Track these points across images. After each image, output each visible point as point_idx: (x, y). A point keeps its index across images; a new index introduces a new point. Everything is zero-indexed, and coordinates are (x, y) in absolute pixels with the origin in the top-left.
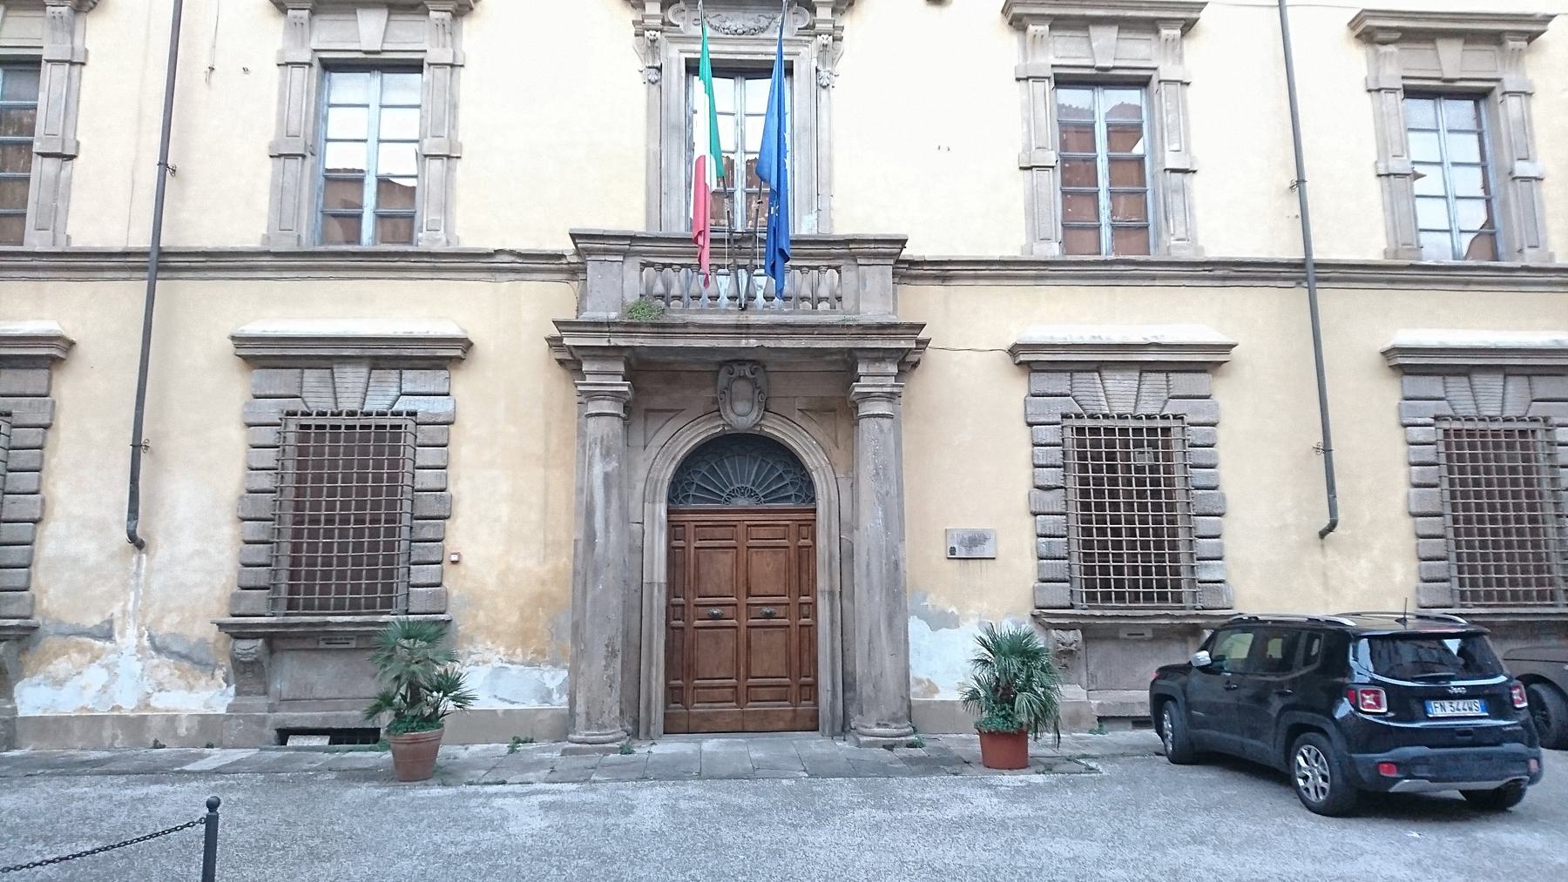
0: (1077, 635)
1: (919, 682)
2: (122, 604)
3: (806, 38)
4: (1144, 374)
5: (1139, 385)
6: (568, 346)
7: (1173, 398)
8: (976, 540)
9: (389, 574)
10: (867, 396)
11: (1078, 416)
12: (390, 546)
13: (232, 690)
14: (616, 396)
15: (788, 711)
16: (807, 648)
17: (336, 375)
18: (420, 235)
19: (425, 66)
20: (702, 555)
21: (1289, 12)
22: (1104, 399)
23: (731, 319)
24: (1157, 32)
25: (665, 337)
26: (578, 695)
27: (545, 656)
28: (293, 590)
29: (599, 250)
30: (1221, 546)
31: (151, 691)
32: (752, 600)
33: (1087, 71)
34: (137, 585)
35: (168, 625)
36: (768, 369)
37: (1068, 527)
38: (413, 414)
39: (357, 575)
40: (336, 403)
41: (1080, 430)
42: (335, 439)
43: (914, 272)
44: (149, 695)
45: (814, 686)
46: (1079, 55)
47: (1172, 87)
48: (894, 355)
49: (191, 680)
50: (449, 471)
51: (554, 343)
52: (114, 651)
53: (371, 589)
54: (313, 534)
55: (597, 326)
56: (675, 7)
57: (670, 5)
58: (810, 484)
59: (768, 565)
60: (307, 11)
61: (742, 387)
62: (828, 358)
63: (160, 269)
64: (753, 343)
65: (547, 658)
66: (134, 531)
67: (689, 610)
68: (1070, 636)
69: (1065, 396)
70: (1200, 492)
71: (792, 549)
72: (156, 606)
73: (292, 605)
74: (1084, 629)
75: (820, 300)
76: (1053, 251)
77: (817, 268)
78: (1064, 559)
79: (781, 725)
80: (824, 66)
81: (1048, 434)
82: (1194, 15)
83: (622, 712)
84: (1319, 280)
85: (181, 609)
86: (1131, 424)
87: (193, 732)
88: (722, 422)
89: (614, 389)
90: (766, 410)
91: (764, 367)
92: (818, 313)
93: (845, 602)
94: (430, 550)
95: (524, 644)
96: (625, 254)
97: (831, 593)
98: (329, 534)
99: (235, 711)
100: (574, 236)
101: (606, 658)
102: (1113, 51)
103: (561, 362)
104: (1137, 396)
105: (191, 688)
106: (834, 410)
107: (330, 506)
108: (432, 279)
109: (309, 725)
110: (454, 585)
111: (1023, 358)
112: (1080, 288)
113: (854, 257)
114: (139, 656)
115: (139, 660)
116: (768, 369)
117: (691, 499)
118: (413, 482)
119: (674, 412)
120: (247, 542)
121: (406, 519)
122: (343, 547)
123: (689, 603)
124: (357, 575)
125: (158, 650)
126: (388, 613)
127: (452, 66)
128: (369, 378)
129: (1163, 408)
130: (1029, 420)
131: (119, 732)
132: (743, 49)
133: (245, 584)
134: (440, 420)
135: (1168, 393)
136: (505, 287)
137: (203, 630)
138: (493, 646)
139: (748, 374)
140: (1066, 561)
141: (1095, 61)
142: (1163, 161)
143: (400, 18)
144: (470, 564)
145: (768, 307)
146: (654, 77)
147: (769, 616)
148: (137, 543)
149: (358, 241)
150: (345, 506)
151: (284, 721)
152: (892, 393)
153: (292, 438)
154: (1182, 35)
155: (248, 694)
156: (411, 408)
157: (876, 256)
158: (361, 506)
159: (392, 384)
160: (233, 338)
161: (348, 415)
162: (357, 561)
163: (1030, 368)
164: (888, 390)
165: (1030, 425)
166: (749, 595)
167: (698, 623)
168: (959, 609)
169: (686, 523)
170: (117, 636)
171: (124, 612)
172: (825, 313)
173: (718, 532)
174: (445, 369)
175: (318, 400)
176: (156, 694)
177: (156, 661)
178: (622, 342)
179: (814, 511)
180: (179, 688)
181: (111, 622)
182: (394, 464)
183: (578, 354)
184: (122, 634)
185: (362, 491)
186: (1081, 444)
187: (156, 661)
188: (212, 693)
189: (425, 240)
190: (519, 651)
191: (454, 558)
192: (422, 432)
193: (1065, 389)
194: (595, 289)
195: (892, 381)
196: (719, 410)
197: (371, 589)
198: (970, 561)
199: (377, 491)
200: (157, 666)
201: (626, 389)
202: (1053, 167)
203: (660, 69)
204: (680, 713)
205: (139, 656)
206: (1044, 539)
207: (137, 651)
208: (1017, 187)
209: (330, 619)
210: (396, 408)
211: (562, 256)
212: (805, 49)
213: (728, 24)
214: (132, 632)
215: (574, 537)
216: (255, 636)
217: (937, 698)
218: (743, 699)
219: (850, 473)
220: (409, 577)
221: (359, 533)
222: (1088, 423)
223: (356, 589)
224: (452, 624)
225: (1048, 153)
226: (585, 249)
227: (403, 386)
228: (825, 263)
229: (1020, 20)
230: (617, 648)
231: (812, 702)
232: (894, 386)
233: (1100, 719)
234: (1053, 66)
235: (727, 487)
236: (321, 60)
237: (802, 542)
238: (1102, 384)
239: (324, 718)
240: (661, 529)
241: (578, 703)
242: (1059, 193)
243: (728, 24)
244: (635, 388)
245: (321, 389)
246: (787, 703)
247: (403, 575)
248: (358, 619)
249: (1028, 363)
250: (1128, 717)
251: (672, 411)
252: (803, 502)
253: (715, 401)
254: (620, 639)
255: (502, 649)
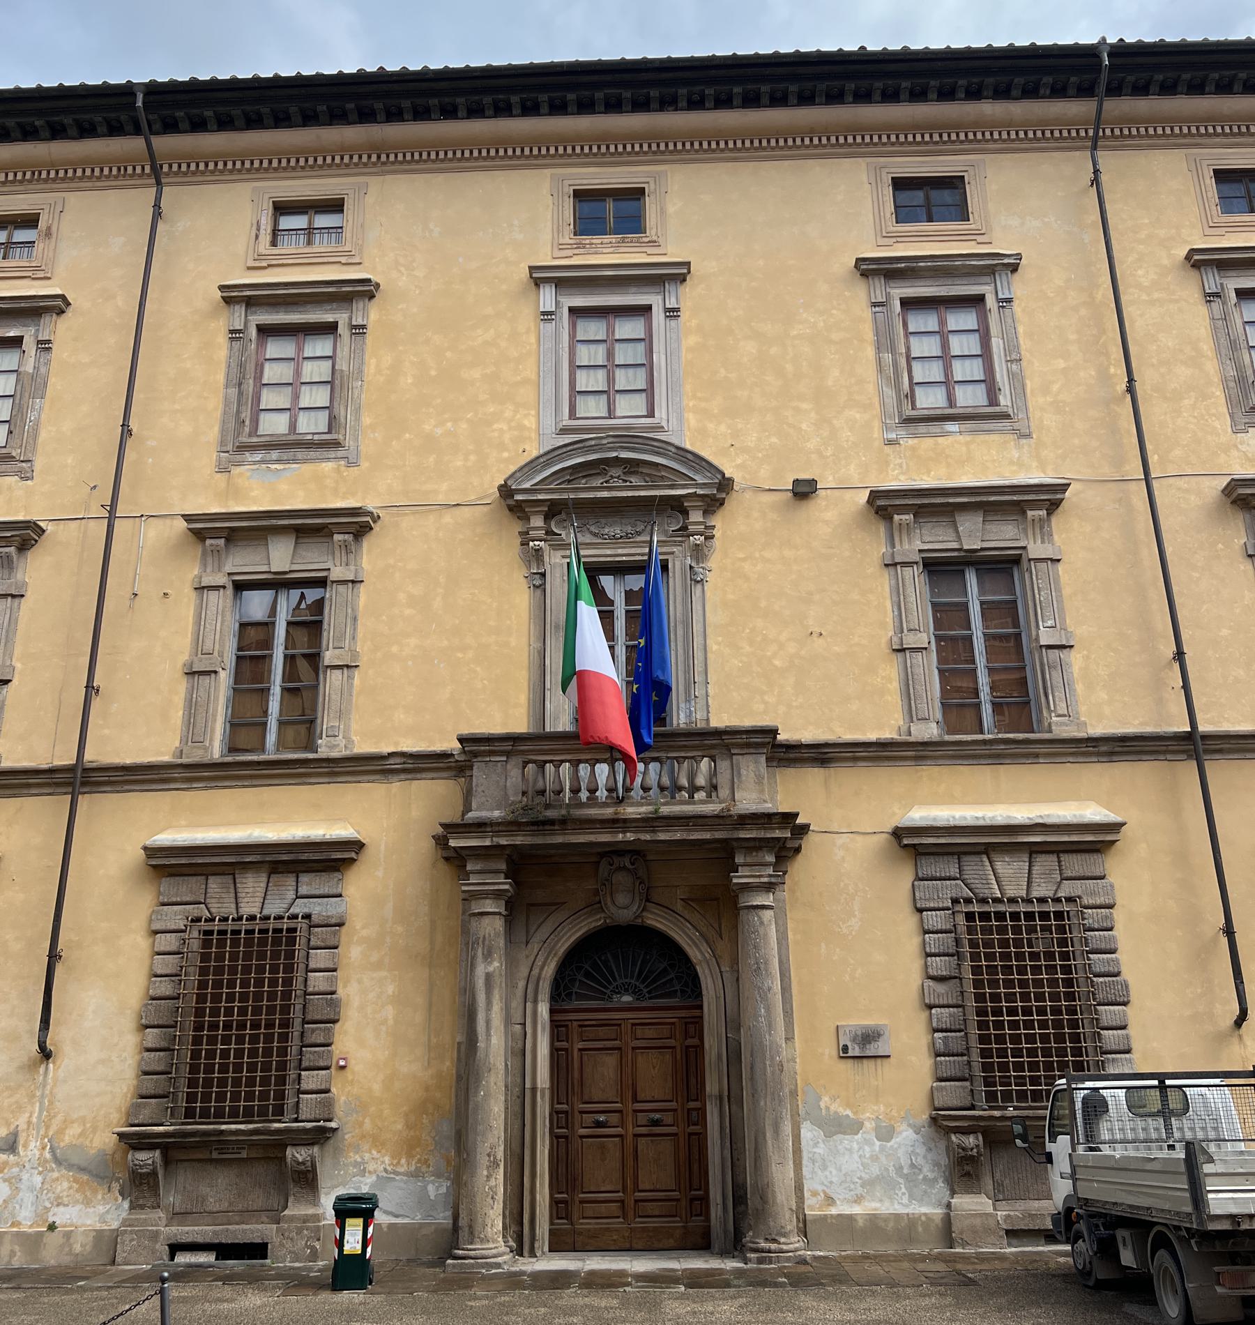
0: (978, 1139)
1: (815, 1194)
2: (27, 1115)
3: (680, 539)
4: (1034, 856)
5: (1030, 866)
6: (454, 848)
7: (1067, 879)
8: (869, 1037)
9: (282, 1081)
10: (747, 888)
11: (968, 901)
12: (283, 1052)
13: (126, 1205)
14: (497, 895)
15: (677, 1227)
16: (697, 1157)
17: (237, 881)
18: (320, 741)
19: (329, 583)
20: (585, 1058)
21: (1155, 484)
22: (994, 882)
23: (608, 812)
24: (1024, 513)
25: (544, 835)
26: (461, 1206)
27: (429, 1166)
28: (191, 1098)
29: (484, 751)
30: (1127, 1037)
31: (48, 1205)
32: (638, 1106)
33: (955, 554)
34: (43, 1096)
35: (71, 1135)
36: (648, 858)
37: (965, 1020)
38: (307, 917)
39: (251, 1082)
40: (237, 909)
41: (970, 916)
42: (235, 943)
43: (792, 756)
44: (47, 1210)
45: (705, 1200)
46: (945, 539)
47: (1042, 566)
48: (771, 845)
49: (88, 1193)
50: (338, 974)
51: (441, 841)
52: (17, 1164)
53: (264, 1096)
54: (212, 1040)
55: (480, 827)
56: (558, 517)
57: (553, 516)
58: (696, 977)
59: (654, 1068)
60: (223, 540)
61: (621, 878)
62: (707, 846)
63: (83, 784)
64: (630, 836)
65: (431, 1169)
66: (45, 1042)
67: (573, 1117)
68: (971, 1141)
69: (954, 879)
70: (1101, 979)
71: (678, 1051)
72: (60, 1117)
73: (189, 1113)
74: (986, 1133)
75: (698, 789)
76: (929, 731)
77: (692, 758)
78: (962, 1055)
79: (671, 1242)
80: (698, 563)
81: (936, 920)
82: (1059, 496)
83: (504, 1227)
84: (1206, 751)
85: (83, 1120)
86: (1023, 908)
87: (88, 1248)
88: (603, 915)
89: (496, 887)
90: (648, 900)
91: (645, 856)
92: (694, 803)
93: (734, 1107)
94: (320, 1055)
95: (410, 1156)
96: (508, 754)
97: (721, 1098)
98: (226, 1040)
99: (130, 1226)
100: (462, 740)
101: (488, 1167)
102: (979, 534)
103: (447, 859)
104: (1029, 878)
105: (87, 1203)
106: (717, 899)
107: (229, 1012)
108: (329, 783)
109: (200, 1239)
110: (341, 1093)
111: (906, 842)
112: (961, 767)
113: (728, 747)
114: (40, 1169)
115: (40, 1173)
116: (648, 858)
117: (574, 997)
118: (305, 986)
119: (558, 905)
120: (148, 1050)
121: (298, 1022)
122: (239, 1053)
123: (573, 1108)
124: (251, 1082)
125: (58, 1161)
126: (279, 1121)
127: (353, 582)
128: (268, 882)
129: (1056, 891)
130: (918, 906)
131: (17, 1248)
132: (620, 551)
133: (144, 1092)
134: (333, 921)
135: (1061, 874)
136: (396, 787)
137: (104, 1140)
138: (379, 1155)
139: (628, 864)
140: (965, 1058)
141: (961, 544)
142: (1037, 639)
143: (306, 540)
144: (356, 1069)
145: (645, 798)
146: (538, 582)
147: (656, 1123)
148: (46, 1054)
149: (262, 749)
150: (242, 1011)
151: (176, 1235)
152: (770, 883)
153: (195, 945)
154: (1049, 514)
155: (142, 1207)
156: (306, 910)
157: (748, 745)
158: (257, 1011)
159: (290, 888)
160: (145, 848)
161: (275, 918)
162: (252, 1068)
163: (918, 852)
164: (766, 880)
165: (920, 911)
166: (635, 1100)
167: (583, 1131)
168: (855, 1113)
169: (569, 1023)
170: (21, 1149)
171: (29, 1123)
172: (702, 802)
173: (602, 1032)
174: (338, 870)
175: (219, 905)
176: (55, 1210)
177: (56, 1175)
178: (503, 841)
179: (701, 1007)
180: (77, 1202)
181: (15, 1135)
182: (289, 968)
183: (464, 853)
184: (25, 1146)
185: (258, 996)
186: (970, 930)
187: (56, 1175)
188: (108, 1207)
189: (326, 748)
190: (403, 1161)
191: (342, 1063)
192: (316, 935)
193: (954, 871)
194: (480, 790)
195: (770, 871)
196: (600, 902)
197: (264, 1096)
198: (865, 1061)
199: (272, 996)
200: (57, 1179)
201: (507, 887)
202: (926, 649)
203: (543, 575)
204: (565, 1230)
205: (40, 1169)
206: (940, 1035)
207: (39, 1164)
208: (889, 673)
209: (224, 1127)
210: (293, 910)
211: (452, 755)
212: (680, 548)
213: (606, 530)
214: (34, 1145)
215: (457, 1040)
216: (151, 1147)
217: (834, 1211)
218: (631, 1213)
219: (735, 966)
220: (299, 1083)
221: (254, 1039)
222: (976, 908)
223: (250, 1096)
224: (340, 1132)
225: (919, 635)
226: (471, 752)
227: (300, 889)
228: (700, 753)
229: (886, 510)
230: (498, 1158)
231: (702, 1218)
232: (770, 876)
233: (1008, 1232)
234: (920, 551)
235: (610, 983)
236: (233, 581)
237: (690, 1042)
238: (991, 866)
239: (215, 1233)
240: (543, 1029)
241: (461, 1216)
242: (936, 672)
243: (606, 530)
244: (517, 883)
245: (223, 895)
246: (678, 1219)
247: (294, 1081)
248: (251, 1126)
249: (914, 846)
250: (1039, 1230)
251: (558, 904)
252: (690, 997)
253: (596, 892)
254: (502, 1148)
255: (387, 1159)
